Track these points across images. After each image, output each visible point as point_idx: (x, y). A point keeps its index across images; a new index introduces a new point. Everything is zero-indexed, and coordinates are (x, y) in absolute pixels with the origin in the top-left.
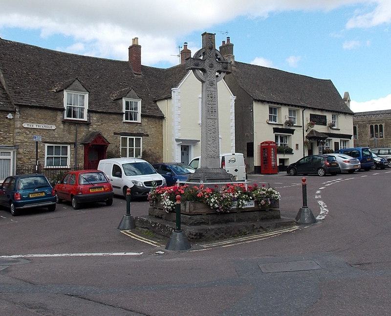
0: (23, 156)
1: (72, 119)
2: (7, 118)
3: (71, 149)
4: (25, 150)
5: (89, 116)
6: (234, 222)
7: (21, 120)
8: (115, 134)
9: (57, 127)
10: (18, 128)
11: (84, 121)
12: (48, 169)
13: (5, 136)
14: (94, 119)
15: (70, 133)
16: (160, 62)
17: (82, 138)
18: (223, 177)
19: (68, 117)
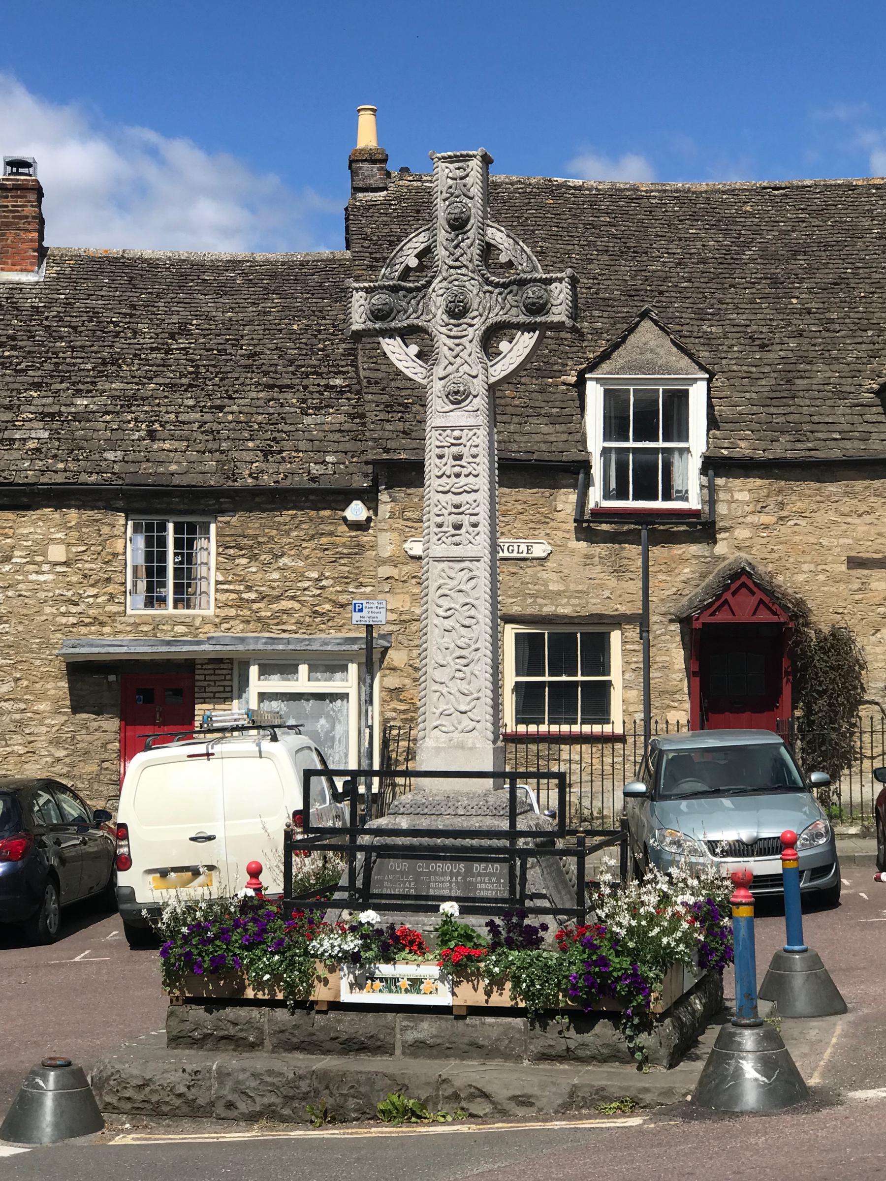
0: (407, 681)
1: (659, 504)
2: (345, 519)
3: (624, 642)
4: (415, 653)
5: (711, 495)
6: (353, 180)
7: (399, 524)
8: (855, 563)
9: (559, 547)
10: (384, 562)
11: (691, 510)
12: (93, 1097)
13: (343, 598)
14: (738, 496)
15: (619, 571)
16: (800, 603)
17: (679, 594)
18: (602, 382)
19: (607, 496)
